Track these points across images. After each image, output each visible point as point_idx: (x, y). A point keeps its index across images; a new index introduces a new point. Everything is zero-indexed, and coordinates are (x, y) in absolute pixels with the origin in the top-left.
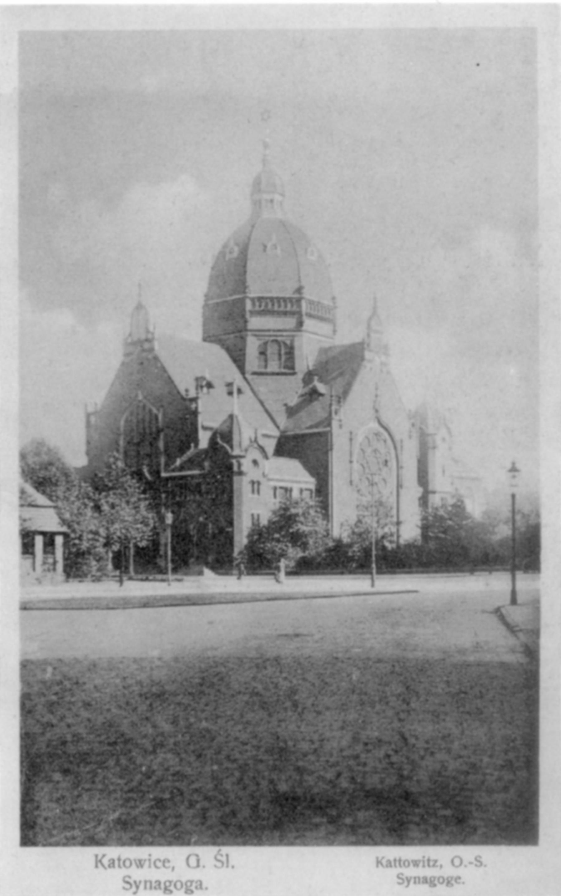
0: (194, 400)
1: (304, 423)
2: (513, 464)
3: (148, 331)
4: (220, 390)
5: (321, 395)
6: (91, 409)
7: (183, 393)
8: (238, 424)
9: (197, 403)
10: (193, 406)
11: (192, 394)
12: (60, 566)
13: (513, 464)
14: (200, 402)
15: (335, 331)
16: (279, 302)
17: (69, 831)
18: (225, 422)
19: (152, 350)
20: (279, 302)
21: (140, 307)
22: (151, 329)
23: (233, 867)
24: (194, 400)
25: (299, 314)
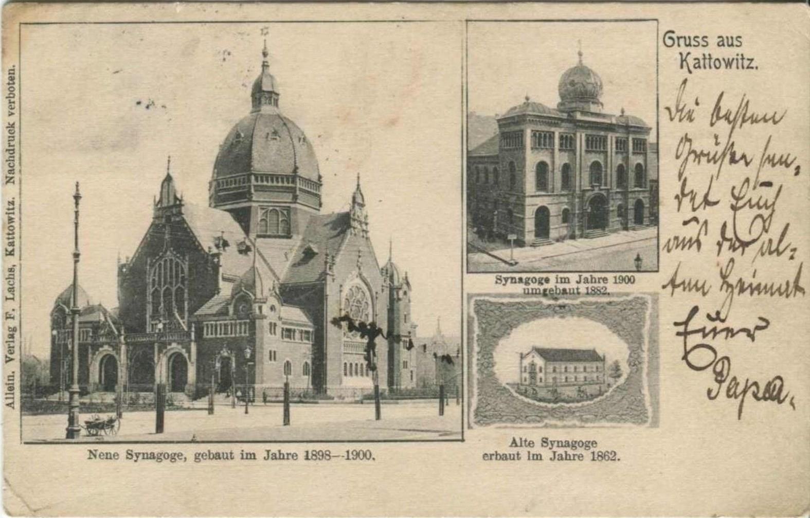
0: (217, 255)
1: (309, 274)
2: (638, 255)
3: (176, 198)
4: (232, 249)
5: (317, 254)
6: (123, 261)
7: (207, 250)
8: (259, 275)
9: (218, 258)
10: (216, 260)
11: (215, 251)
12: (17, 405)
13: (638, 255)
14: (221, 257)
15: (320, 205)
16: (277, 179)
17: (473, 357)
18: (247, 272)
19: (180, 213)
20: (277, 179)
21: (169, 179)
22: (179, 196)
23: (374, 459)
24: (217, 255)
25: (292, 190)
